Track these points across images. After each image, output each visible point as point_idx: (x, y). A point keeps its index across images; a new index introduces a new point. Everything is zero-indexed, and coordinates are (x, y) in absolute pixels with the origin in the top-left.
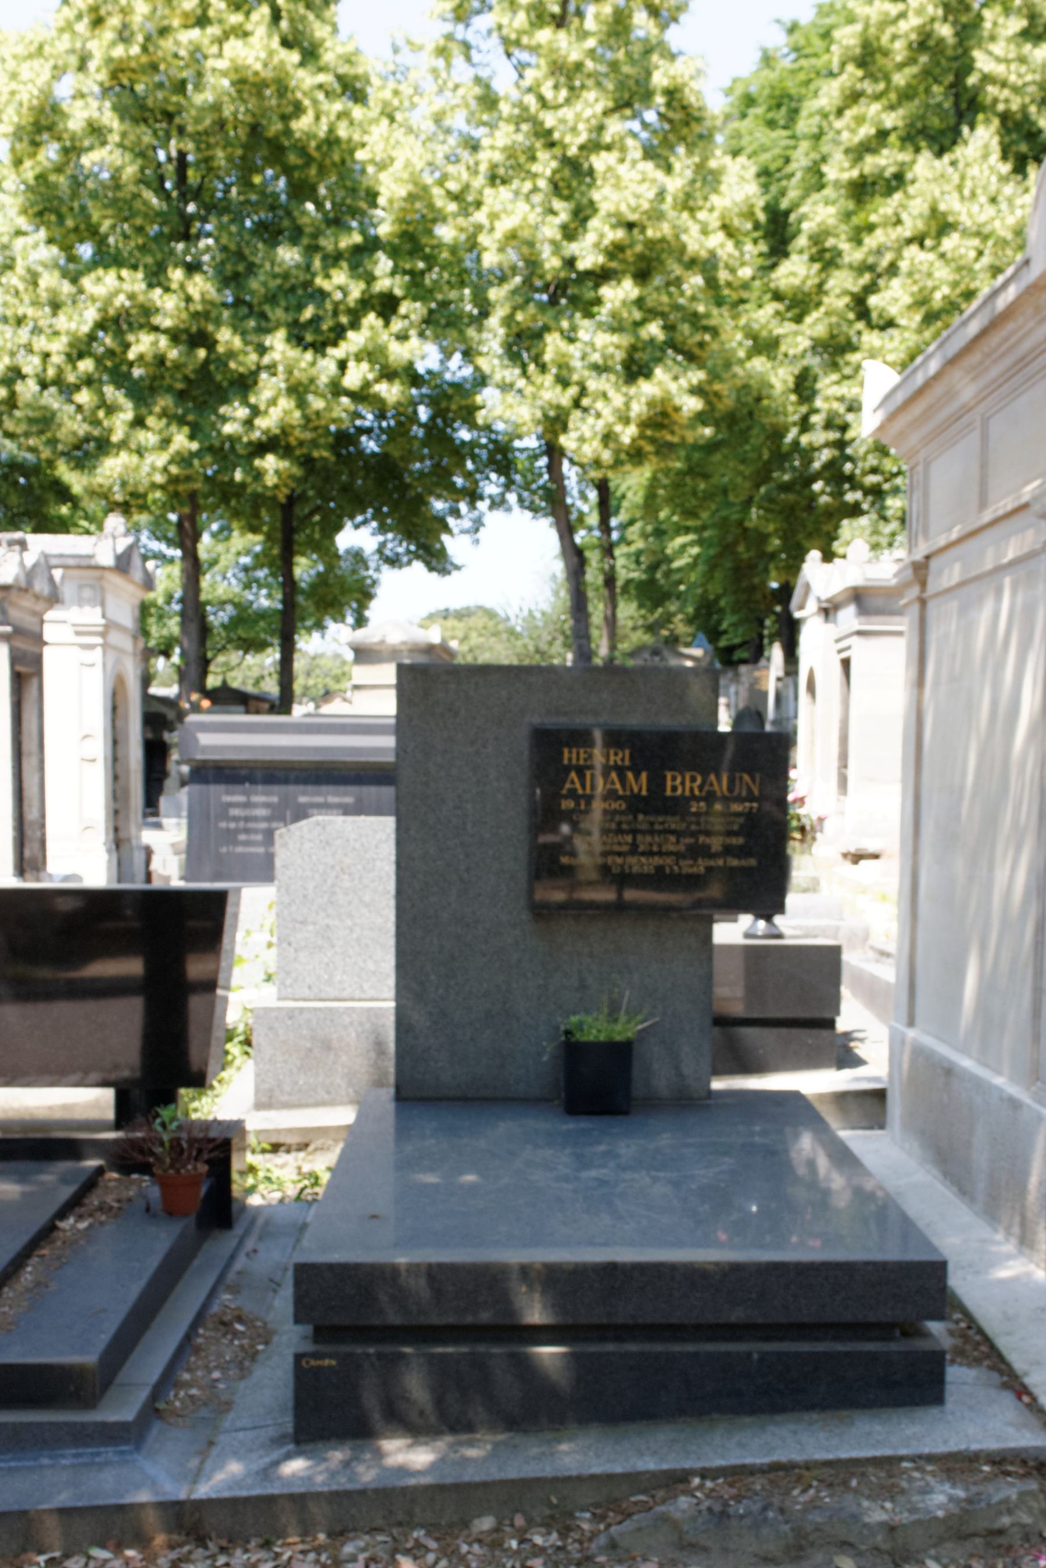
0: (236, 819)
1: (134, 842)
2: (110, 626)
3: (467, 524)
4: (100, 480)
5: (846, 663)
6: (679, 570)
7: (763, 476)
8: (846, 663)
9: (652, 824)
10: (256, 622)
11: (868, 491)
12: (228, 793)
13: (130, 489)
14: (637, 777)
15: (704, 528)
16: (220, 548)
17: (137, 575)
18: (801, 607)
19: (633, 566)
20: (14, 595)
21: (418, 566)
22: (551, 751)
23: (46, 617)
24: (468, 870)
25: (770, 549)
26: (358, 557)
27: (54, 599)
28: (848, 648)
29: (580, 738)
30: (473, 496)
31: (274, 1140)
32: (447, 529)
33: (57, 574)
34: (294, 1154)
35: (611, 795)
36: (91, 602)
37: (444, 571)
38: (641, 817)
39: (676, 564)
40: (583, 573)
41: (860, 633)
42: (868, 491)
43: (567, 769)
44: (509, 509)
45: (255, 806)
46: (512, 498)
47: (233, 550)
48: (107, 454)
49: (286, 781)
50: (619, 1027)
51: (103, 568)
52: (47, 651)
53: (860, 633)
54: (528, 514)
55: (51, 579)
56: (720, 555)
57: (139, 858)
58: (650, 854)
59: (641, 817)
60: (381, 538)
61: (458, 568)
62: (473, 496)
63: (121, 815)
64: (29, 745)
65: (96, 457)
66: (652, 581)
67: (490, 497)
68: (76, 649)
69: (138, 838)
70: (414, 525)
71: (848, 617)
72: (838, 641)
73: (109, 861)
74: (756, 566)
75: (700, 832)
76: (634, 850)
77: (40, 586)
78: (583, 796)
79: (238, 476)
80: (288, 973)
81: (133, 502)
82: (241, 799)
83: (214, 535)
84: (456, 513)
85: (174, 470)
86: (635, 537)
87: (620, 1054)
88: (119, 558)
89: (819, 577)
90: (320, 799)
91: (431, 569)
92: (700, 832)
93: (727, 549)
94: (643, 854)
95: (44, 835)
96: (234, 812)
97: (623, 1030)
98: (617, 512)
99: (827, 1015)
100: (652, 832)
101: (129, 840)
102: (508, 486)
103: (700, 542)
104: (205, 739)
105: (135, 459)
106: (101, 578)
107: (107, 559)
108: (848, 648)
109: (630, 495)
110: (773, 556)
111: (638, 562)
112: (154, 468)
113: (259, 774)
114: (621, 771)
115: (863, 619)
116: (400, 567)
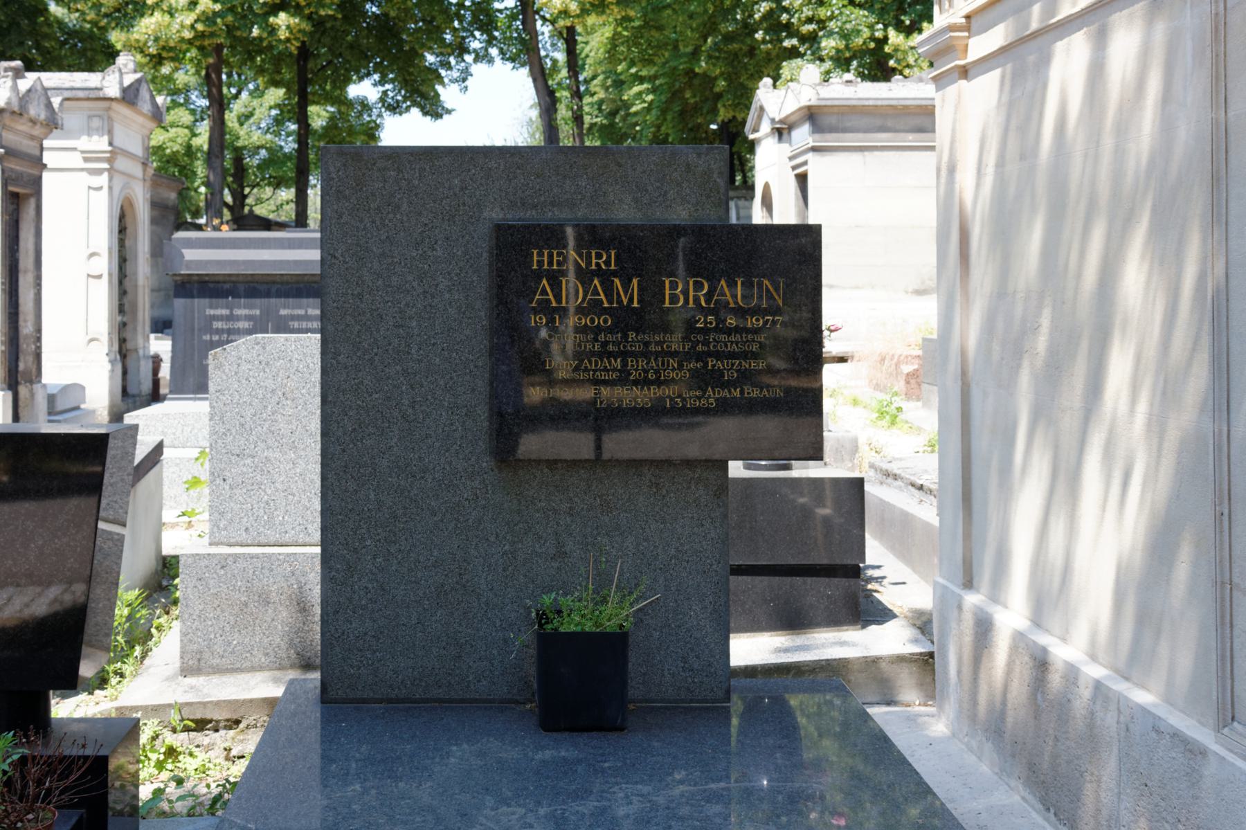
0: (218, 331)
1: (141, 352)
2: (115, 152)
3: (455, 74)
4: (136, 36)
5: (802, 179)
6: (636, 114)
7: (710, 27)
8: (802, 179)
9: (647, 344)
10: (284, 163)
11: (803, 39)
12: (211, 307)
13: (162, 43)
14: (626, 285)
15: (655, 77)
16: (255, 103)
17: (146, 107)
18: (756, 130)
19: (596, 112)
20: (7, 118)
21: (415, 111)
22: (517, 256)
23: (46, 143)
24: (412, 405)
25: (717, 90)
26: (365, 105)
27: (52, 124)
28: (805, 163)
29: (551, 236)
30: (462, 49)
31: (198, 716)
32: (439, 79)
33: (56, 101)
34: (222, 732)
35: (594, 307)
36: (99, 131)
37: (437, 116)
38: (632, 335)
39: (634, 109)
40: (556, 111)
41: (814, 149)
42: (803, 39)
43: (539, 275)
44: (491, 61)
45: (238, 318)
46: (494, 52)
47: (266, 105)
48: (142, 15)
49: (268, 295)
50: (609, 609)
51: (111, 99)
52: (46, 176)
53: (814, 149)
54: (510, 65)
55: (49, 105)
56: (670, 101)
57: (146, 368)
58: (644, 382)
59: (632, 335)
60: (381, 89)
61: (449, 112)
62: (462, 49)
63: (129, 327)
64: (26, 261)
65: (133, 18)
66: (612, 125)
67: (475, 51)
68: (84, 174)
69: (146, 348)
70: (411, 74)
71: (803, 135)
72: (791, 158)
73: (112, 371)
74: (701, 108)
75: (709, 354)
76: (623, 379)
77: (36, 110)
78: (555, 310)
79: (256, 32)
80: (222, 514)
81: (164, 54)
82: (225, 312)
83: (251, 93)
84: (448, 67)
85: (200, 27)
86: (597, 89)
87: (609, 649)
88: (125, 91)
89: (773, 100)
90: (301, 312)
91: (425, 113)
92: (709, 354)
93: (676, 95)
94: (636, 383)
95: (39, 348)
96: (218, 325)
97: (615, 615)
98: (583, 69)
99: (849, 561)
100: (646, 355)
101: (136, 350)
102: (490, 41)
103: (653, 91)
104: (190, 254)
105: (167, 17)
106: (109, 109)
107: (113, 90)
108: (805, 163)
109: (592, 54)
110: (719, 96)
111: (600, 109)
112: (182, 26)
113: (241, 288)
114: (606, 277)
115: (817, 136)
116: (401, 114)
